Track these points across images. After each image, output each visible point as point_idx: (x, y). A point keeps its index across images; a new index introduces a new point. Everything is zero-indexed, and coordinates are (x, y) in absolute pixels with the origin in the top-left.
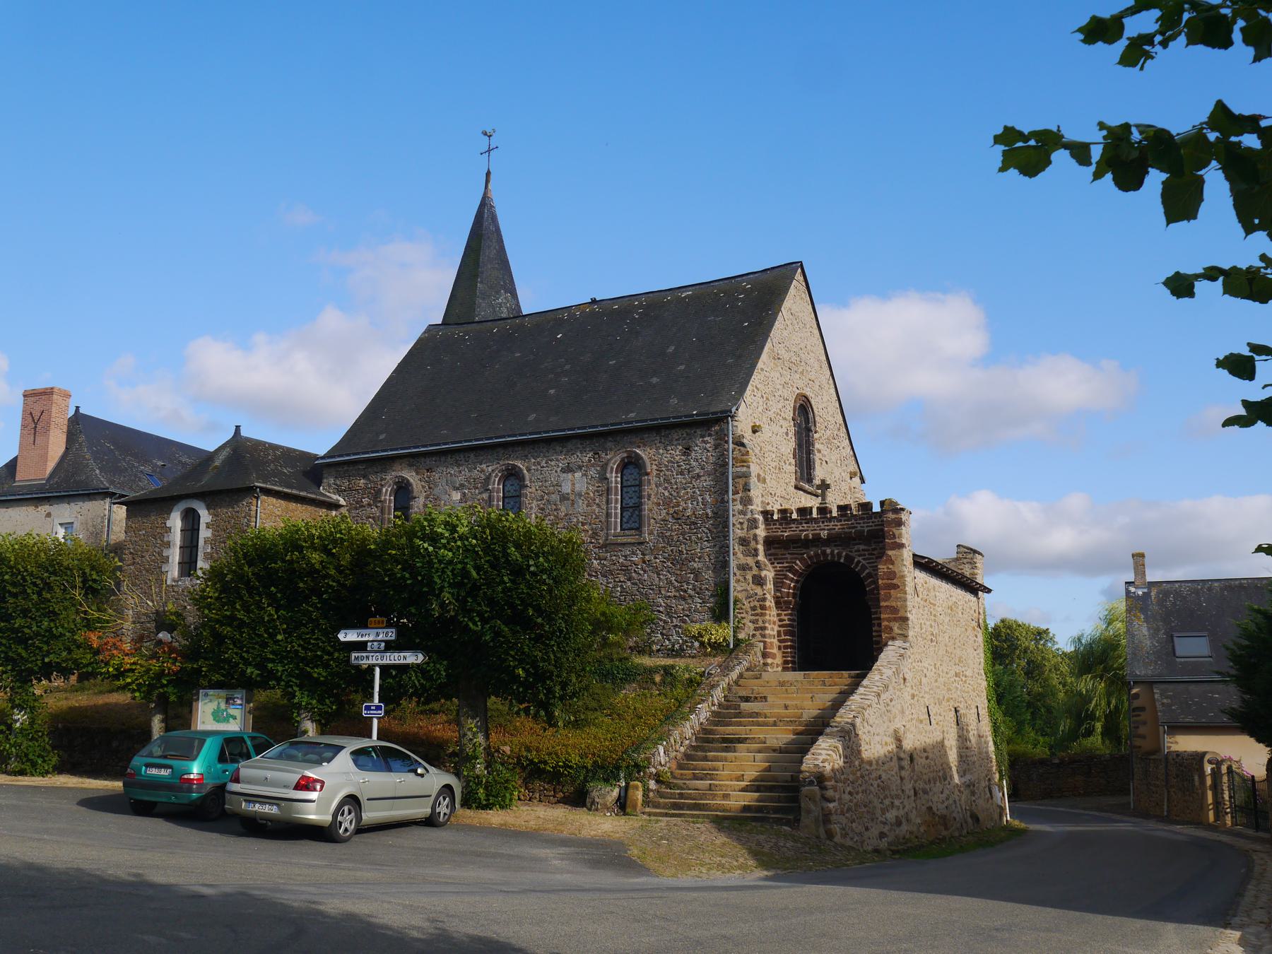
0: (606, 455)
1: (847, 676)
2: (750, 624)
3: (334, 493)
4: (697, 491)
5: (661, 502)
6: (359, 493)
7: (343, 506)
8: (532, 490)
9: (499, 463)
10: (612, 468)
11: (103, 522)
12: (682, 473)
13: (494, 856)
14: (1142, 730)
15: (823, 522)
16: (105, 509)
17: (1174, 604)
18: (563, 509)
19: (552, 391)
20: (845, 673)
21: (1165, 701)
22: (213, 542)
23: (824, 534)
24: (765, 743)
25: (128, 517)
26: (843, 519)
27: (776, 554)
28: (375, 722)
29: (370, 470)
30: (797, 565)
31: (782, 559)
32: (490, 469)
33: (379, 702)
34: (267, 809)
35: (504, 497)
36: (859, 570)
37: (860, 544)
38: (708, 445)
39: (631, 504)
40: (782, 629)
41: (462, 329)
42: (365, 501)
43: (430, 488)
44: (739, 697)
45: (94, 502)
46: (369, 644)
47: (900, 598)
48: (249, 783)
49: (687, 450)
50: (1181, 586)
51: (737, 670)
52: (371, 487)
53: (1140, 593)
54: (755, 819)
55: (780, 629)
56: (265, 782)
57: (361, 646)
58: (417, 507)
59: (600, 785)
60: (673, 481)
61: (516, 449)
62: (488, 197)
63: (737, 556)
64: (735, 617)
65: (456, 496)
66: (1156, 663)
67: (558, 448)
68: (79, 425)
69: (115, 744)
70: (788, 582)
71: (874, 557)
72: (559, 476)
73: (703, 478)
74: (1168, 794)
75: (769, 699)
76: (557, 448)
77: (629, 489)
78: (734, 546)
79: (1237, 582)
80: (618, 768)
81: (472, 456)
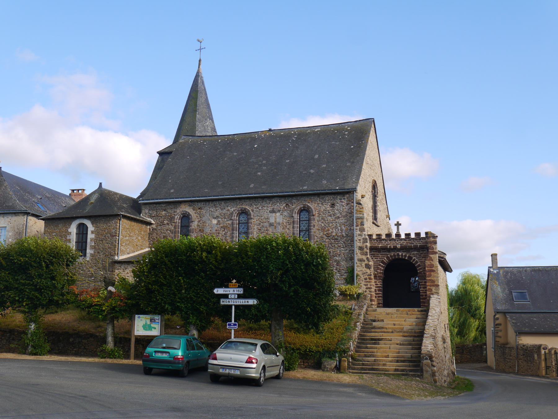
0: (293, 205)
1: (417, 311)
2: (364, 286)
3: (148, 217)
4: (338, 224)
5: (320, 229)
6: (162, 218)
7: (153, 224)
8: (254, 221)
9: (237, 207)
10: (295, 212)
11: (23, 227)
12: (330, 216)
13: (80, 396)
14: (500, 334)
15: (398, 241)
16: (24, 221)
17: (511, 277)
18: (270, 230)
19: (259, 173)
20: (416, 309)
21: (513, 321)
22: (96, 240)
23: (399, 246)
24: (391, 341)
25: (46, 226)
26: (407, 240)
27: (375, 255)
28: (233, 331)
29: (168, 207)
30: (384, 259)
31: (377, 257)
32: (232, 209)
33: (234, 322)
34: (232, 372)
35: (239, 223)
36: (415, 263)
37: (414, 251)
38: (344, 203)
39: (304, 229)
40: (377, 288)
41: (201, 139)
42: (166, 222)
43: (200, 217)
44: (371, 320)
45: (18, 217)
46: (230, 295)
47: (436, 276)
48: (219, 360)
49: (333, 205)
50: (513, 269)
51: (365, 307)
52: (169, 216)
53: (495, 272)
54: (403, 375)
55: (376, 288)
56: (231, 360)
57: (226, 296)
58: (194, 226)
59: (329, 360)
60: (326, 219)
61: (246, 201)
62: (200, 72)
63: (358, 255)
64: (357, 283)
65: (215, 222)
66: (505, 304)
67: (268, 201)
68: (3, 177)
69: (71, 340)
70: (380, 267)
71: (421, 257)
72: (268, 214)
73: (341, 218)
74: (518, 363)
75: (384, 321)
76: (267, 201)
77: (303, 222)
78: (357, 251)
79: (537, 268)
80: (335, 352)
81: (223, 203)
